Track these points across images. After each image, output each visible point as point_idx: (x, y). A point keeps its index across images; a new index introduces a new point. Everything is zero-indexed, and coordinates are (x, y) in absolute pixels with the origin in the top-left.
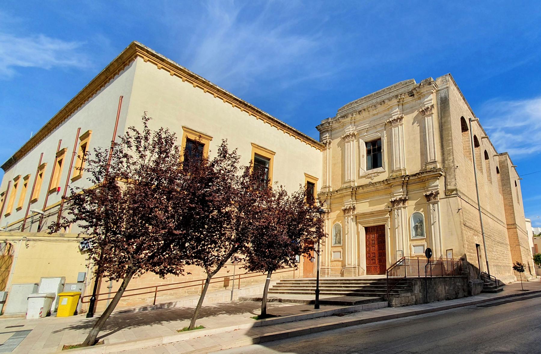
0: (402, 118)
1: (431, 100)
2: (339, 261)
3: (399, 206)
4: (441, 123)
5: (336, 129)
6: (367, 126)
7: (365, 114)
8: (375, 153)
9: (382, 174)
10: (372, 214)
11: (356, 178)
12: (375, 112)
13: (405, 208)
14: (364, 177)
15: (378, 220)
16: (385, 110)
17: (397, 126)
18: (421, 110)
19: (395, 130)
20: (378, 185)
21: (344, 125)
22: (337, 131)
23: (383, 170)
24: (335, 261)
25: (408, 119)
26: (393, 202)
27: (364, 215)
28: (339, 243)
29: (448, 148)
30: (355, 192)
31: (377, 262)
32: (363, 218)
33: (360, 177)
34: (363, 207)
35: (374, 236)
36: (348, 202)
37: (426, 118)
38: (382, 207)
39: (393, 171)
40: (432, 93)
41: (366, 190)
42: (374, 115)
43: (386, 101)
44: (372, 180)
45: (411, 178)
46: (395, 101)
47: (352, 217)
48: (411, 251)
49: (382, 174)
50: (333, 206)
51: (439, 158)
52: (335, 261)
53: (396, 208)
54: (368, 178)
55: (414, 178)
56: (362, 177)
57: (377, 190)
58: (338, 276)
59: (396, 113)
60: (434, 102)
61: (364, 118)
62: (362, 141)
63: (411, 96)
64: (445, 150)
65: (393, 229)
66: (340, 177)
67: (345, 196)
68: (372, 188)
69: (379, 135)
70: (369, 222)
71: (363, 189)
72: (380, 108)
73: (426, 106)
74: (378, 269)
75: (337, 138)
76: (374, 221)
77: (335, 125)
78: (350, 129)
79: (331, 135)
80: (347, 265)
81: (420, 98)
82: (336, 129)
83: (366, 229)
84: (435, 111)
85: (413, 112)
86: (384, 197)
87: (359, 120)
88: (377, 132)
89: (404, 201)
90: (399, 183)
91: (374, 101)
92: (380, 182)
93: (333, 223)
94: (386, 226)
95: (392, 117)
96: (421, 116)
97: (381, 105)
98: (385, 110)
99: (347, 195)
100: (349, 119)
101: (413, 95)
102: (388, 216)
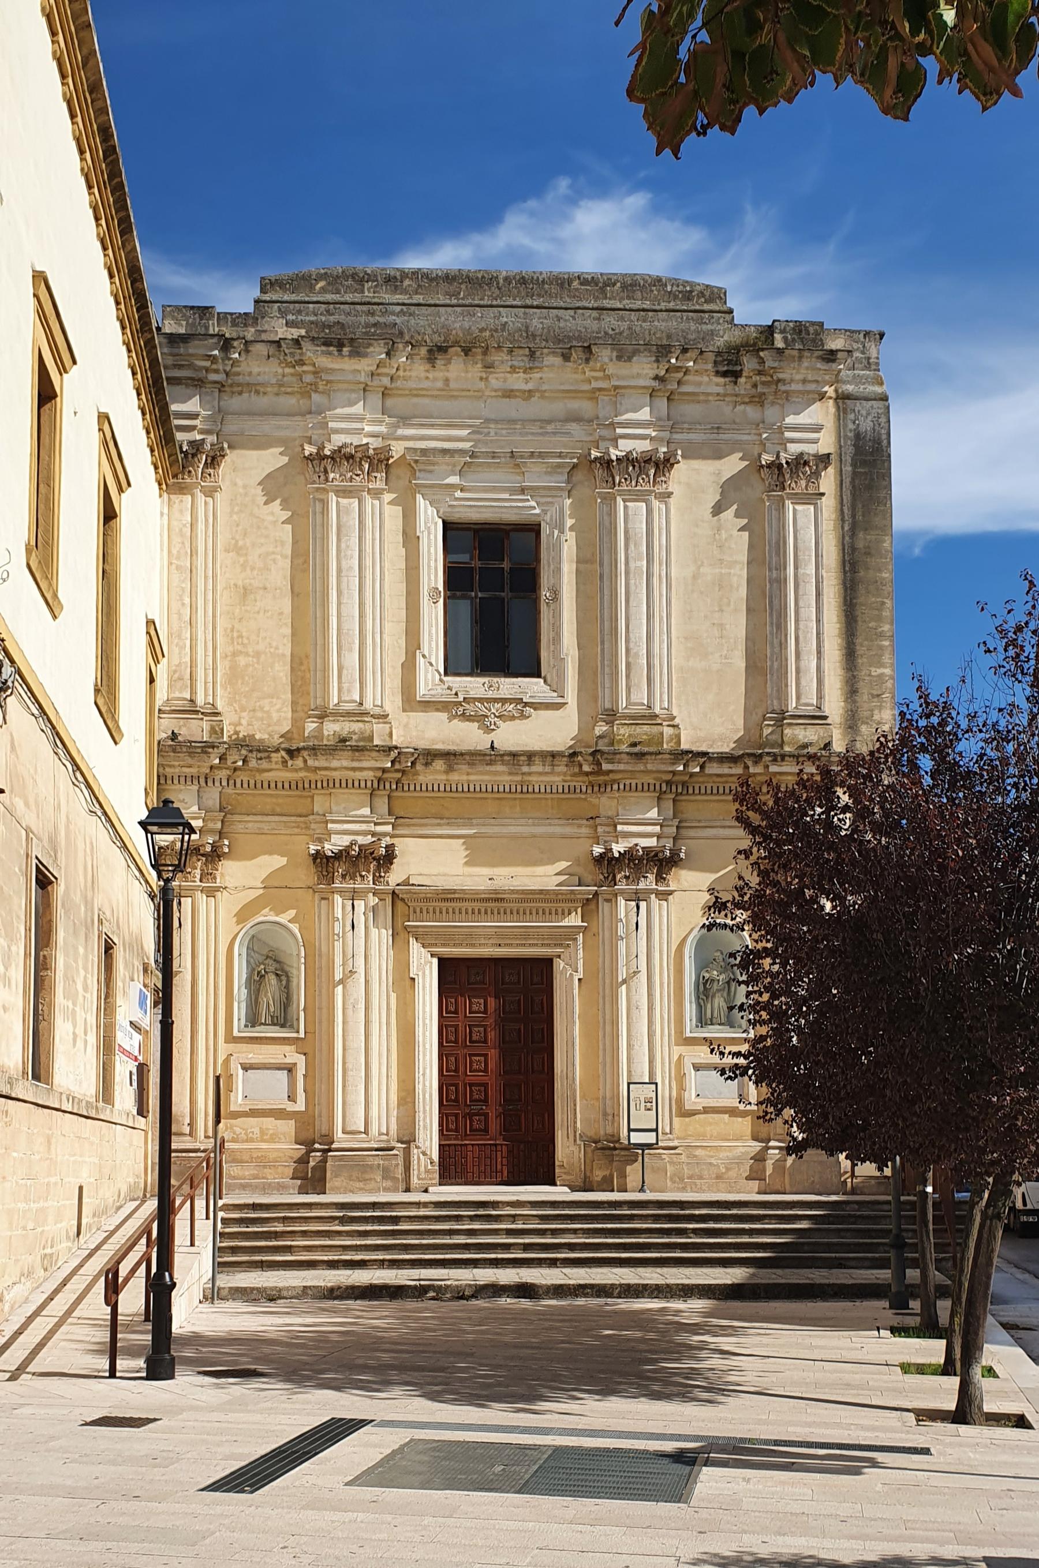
0: (664, 465)
1: (817, 428)
2: (279, 1114)
3: (642, 885)
4: (853, 549)
5: (254, 388)
6: (459, 438)
7: (458, 370)
8: (495, 601)
9: (544, 718)
10: (495, 902)
11: (392, 704)
12: (518, 382)
13: (664, 896)
14: (427, 705)
15: (525, 935)
16: (573, 394)
17: (641, 496)
18: (766, 458)
19: (631, 514)
20: (537, 768)
21: (315, 387)
22: (262, 402)
23: (552, 697)
24: (253, 1113)
25: (696, 480)
26: (608, 864)
27: (448, 900)
28: (283, 1019)
29: (876, 671)
30: (401, 778)
31: (494, 1126)
32: (437, 914)
33: (411, 702)
34: (431, 860)
35: (481, 1007)
36: (349, 826)
37: (790, 506)
38: (545, 876)
39: (611, 715)
40: (822, 396)
41: (460, 776)
42: (509, 394)
43: (604, 354)
44: (488, 730)
45: (713, 769)
46: (643, 369)
47: (373, 900)
48: (682, 1088)
49: (544, 718)
50: (243, 825)
51: (834, 707)
52: (253, 1113)
53: (622, 892)
54: (465, 717)
55: (725, 769)
56: (427, 705)
57: (524, 791)
58: (281, 1188)
59: (636, 433)
60: (826, 443)
61: (447, 392)
62: (431, 511)
63: (724, 374)
64: (863, 674)
65: (603, 986)
66: (282, 672)
67: (330, 785)
68: (501, 775)
69: (530, 508)
70: (469, 937)
71: (450, 769)
72: (555, 373)
73: (794, 448)
74: (501, 1160)
75: (260, 443)
76: (501, 937)
77: (258, 366)
78: (355, 424)
79: (221, 414)
80: (339, 1134)
81: (758, 400)
82: (254, 388)
83: (444, 964)
84: (828, 481)
85: (718, 455)
86: (558, 830)
87: (415, 393)
88: (523, 490)
89: (662, 862)
90: (649, 779)
91: (537, 321)
92: (553, 755)
93: (242, 916)
94: (559, 965)
95: (615, 440)
96: (757, 489)
97: (566, 358)
98: (573, 394)
99: (349, 784)
100: (365, 365)
101: (736, 375)
102: (574, 920)
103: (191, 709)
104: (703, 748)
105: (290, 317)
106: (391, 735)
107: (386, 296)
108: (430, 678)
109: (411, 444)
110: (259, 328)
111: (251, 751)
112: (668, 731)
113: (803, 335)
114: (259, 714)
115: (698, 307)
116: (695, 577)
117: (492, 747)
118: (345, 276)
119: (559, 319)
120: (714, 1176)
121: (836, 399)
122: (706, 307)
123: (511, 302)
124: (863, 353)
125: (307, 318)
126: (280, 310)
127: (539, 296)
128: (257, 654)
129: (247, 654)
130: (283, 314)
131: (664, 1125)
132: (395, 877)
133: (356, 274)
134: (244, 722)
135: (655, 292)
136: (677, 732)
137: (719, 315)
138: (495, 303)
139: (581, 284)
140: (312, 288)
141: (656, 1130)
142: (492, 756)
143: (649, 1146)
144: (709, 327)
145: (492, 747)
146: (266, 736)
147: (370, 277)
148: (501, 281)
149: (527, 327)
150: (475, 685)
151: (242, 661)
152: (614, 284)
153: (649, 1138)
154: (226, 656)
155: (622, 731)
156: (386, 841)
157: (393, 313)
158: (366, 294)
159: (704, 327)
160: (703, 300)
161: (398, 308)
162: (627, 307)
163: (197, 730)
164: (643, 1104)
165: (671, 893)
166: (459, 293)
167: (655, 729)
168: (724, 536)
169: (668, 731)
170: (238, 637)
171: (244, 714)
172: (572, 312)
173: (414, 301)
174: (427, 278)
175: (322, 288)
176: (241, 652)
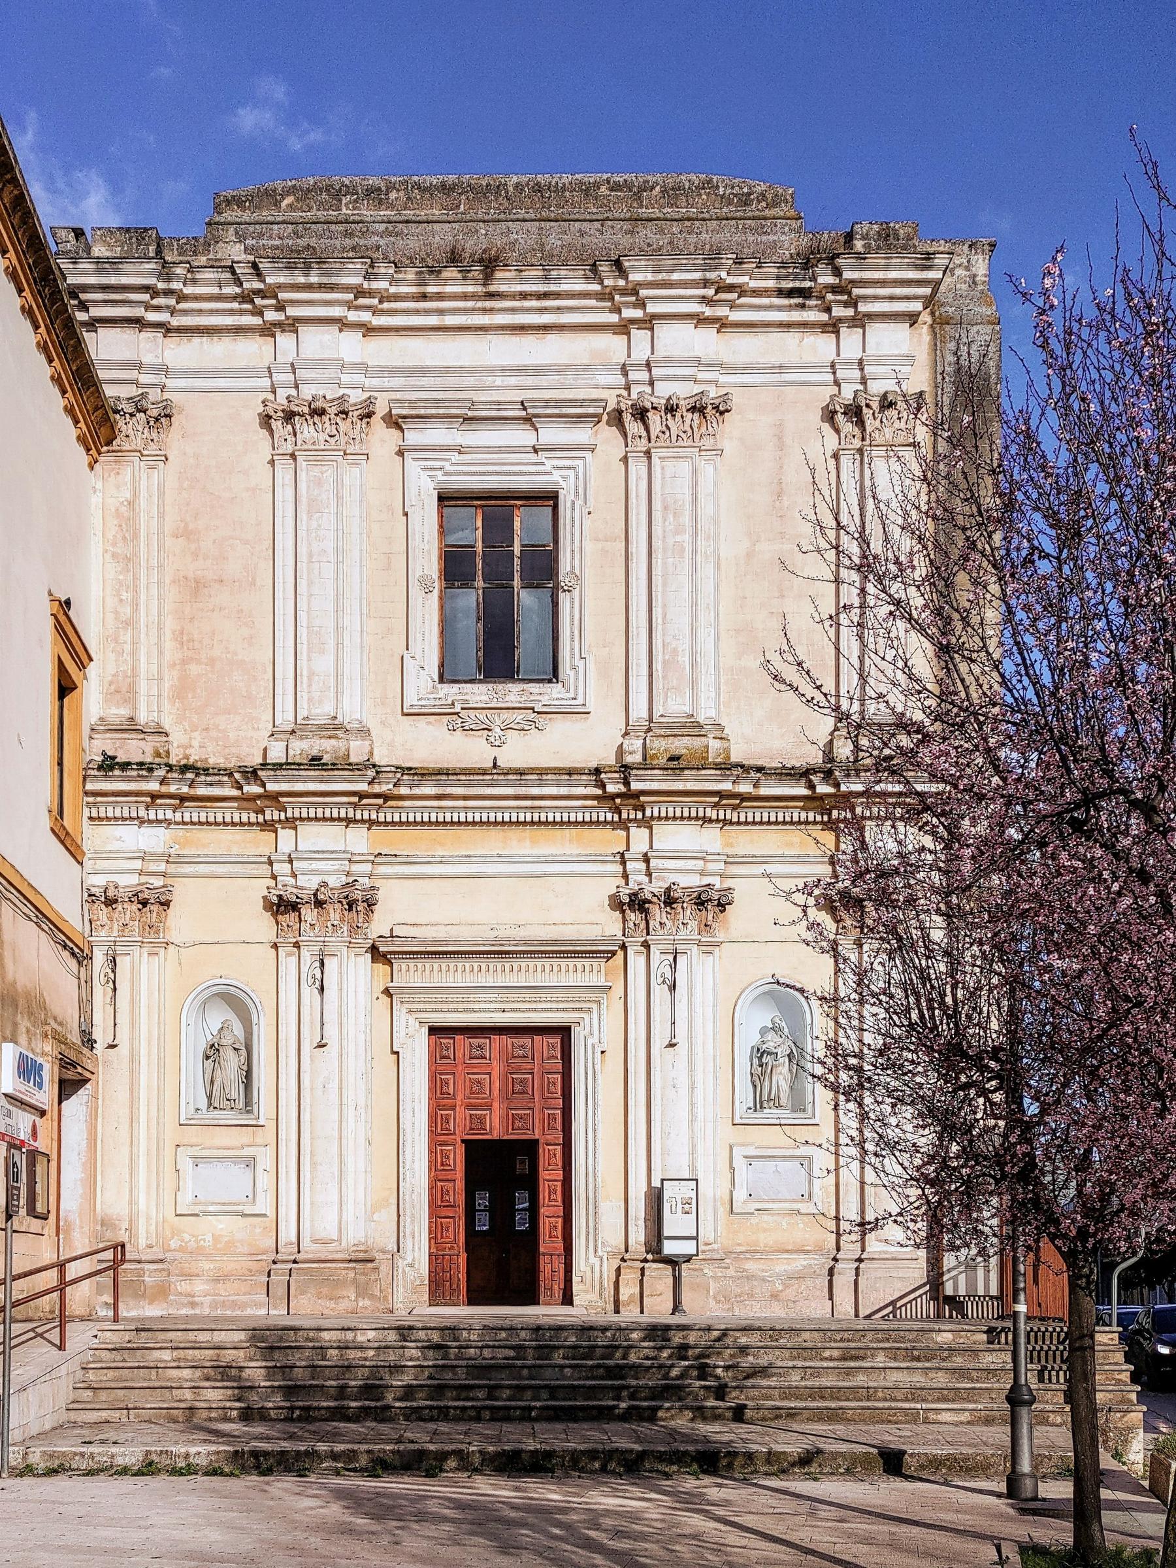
8: (499, 585)
19: (674, 472)
91: (555, 237)
103: (131, 727)
104: (760, 763)
105: (250, 242)
106: (371, 753)
107: (368, 213)
108: (422, 682)
109: (394, 395)
110: (211, 256)
111: (866, 1152)
112: (714, 745)
113: (891, 240)
114: (214, 734)
115: (757, 213)
116: (749, 555)
117: (495, 766)
118: (316, 189)
119: (582, 234)
120: (768, 1294)
121: (931, 326)
122: (767, 213)
123: (522, 214)
124: (967, 269)
125: (271, 243)
126: (237, 232)
127: (558, 206)
128: (212, 662)
129: (199, 662)
130: (241, 238)
131: (706, 1234)
132: (379, 926)
133: (332, 186)
134: (195, 743)
135: (704, 197)
136: (726, 745)
137: (784, 221)
138: (502, 216)
139: (611, 189)
140: (277, 204)
141: (696, 1238)
142: (495, 772)
143: (688, 1259)
144: (771, 238)
145: (495, 766)
146: (222, 760)
147: (351, 190)
148: (511, 189)
149: (542, 245)
150: (480, 693)
151: (194, 669)
152: (653, 188)
153: (688, 1248)
154: (175, 664)
155: (656, 744)
156: (365, 882)
157: (375, 233)
158: (344, 211)
159: (764, 238)
160: (764, 204)
161: (382, 227)
162: (668, 216)
163: (133, 750)
164: (680, 1206)
165: (719, 944)
166: (458, 207)
167: (698, 742)
168: (786, 504)
169: (714, 745)
170: (188, 641)
171: (196, 734)
172: (597, 225)
173: (403, 218)
174: (419, 188)
175: (290, 206)
176: (192, 659)
